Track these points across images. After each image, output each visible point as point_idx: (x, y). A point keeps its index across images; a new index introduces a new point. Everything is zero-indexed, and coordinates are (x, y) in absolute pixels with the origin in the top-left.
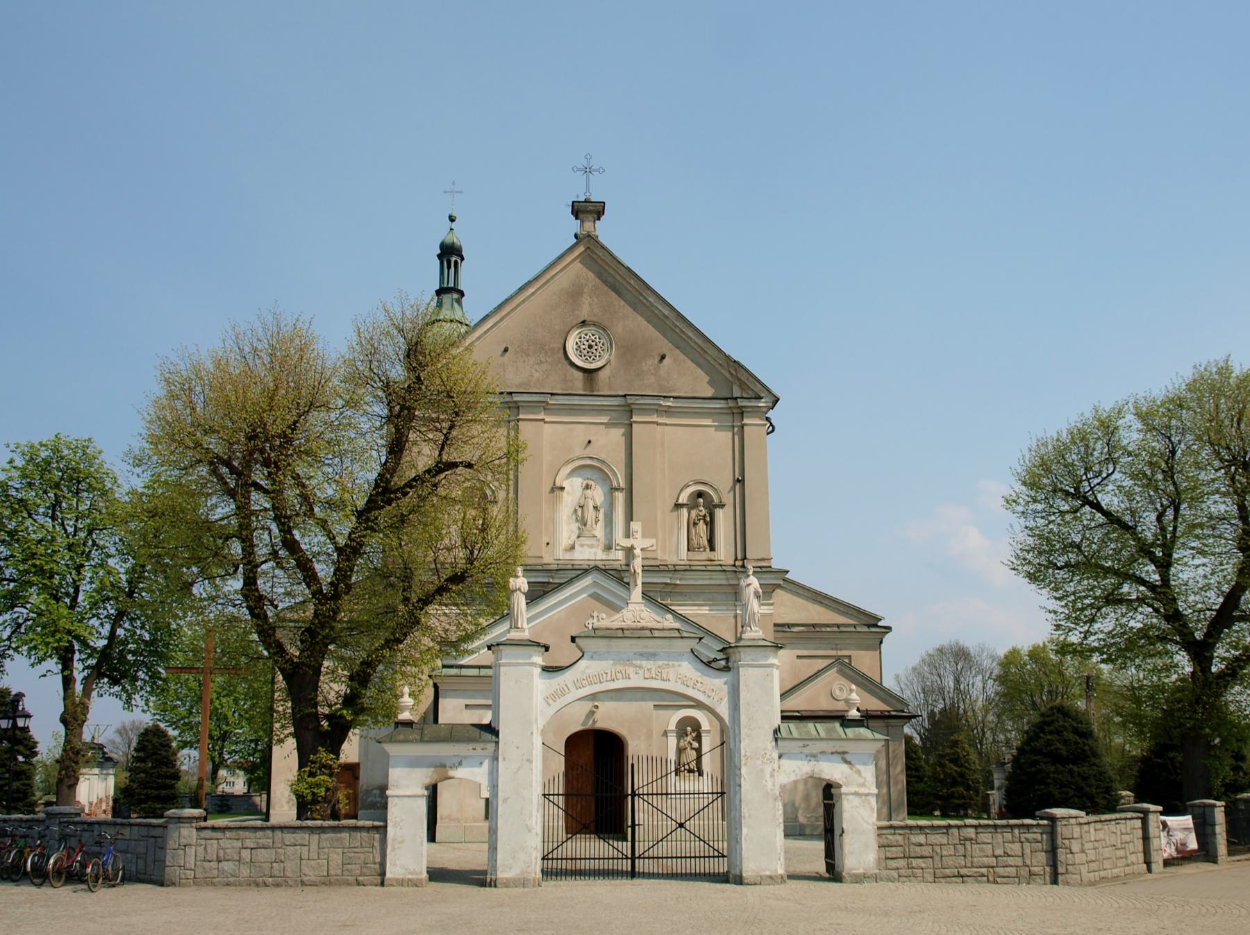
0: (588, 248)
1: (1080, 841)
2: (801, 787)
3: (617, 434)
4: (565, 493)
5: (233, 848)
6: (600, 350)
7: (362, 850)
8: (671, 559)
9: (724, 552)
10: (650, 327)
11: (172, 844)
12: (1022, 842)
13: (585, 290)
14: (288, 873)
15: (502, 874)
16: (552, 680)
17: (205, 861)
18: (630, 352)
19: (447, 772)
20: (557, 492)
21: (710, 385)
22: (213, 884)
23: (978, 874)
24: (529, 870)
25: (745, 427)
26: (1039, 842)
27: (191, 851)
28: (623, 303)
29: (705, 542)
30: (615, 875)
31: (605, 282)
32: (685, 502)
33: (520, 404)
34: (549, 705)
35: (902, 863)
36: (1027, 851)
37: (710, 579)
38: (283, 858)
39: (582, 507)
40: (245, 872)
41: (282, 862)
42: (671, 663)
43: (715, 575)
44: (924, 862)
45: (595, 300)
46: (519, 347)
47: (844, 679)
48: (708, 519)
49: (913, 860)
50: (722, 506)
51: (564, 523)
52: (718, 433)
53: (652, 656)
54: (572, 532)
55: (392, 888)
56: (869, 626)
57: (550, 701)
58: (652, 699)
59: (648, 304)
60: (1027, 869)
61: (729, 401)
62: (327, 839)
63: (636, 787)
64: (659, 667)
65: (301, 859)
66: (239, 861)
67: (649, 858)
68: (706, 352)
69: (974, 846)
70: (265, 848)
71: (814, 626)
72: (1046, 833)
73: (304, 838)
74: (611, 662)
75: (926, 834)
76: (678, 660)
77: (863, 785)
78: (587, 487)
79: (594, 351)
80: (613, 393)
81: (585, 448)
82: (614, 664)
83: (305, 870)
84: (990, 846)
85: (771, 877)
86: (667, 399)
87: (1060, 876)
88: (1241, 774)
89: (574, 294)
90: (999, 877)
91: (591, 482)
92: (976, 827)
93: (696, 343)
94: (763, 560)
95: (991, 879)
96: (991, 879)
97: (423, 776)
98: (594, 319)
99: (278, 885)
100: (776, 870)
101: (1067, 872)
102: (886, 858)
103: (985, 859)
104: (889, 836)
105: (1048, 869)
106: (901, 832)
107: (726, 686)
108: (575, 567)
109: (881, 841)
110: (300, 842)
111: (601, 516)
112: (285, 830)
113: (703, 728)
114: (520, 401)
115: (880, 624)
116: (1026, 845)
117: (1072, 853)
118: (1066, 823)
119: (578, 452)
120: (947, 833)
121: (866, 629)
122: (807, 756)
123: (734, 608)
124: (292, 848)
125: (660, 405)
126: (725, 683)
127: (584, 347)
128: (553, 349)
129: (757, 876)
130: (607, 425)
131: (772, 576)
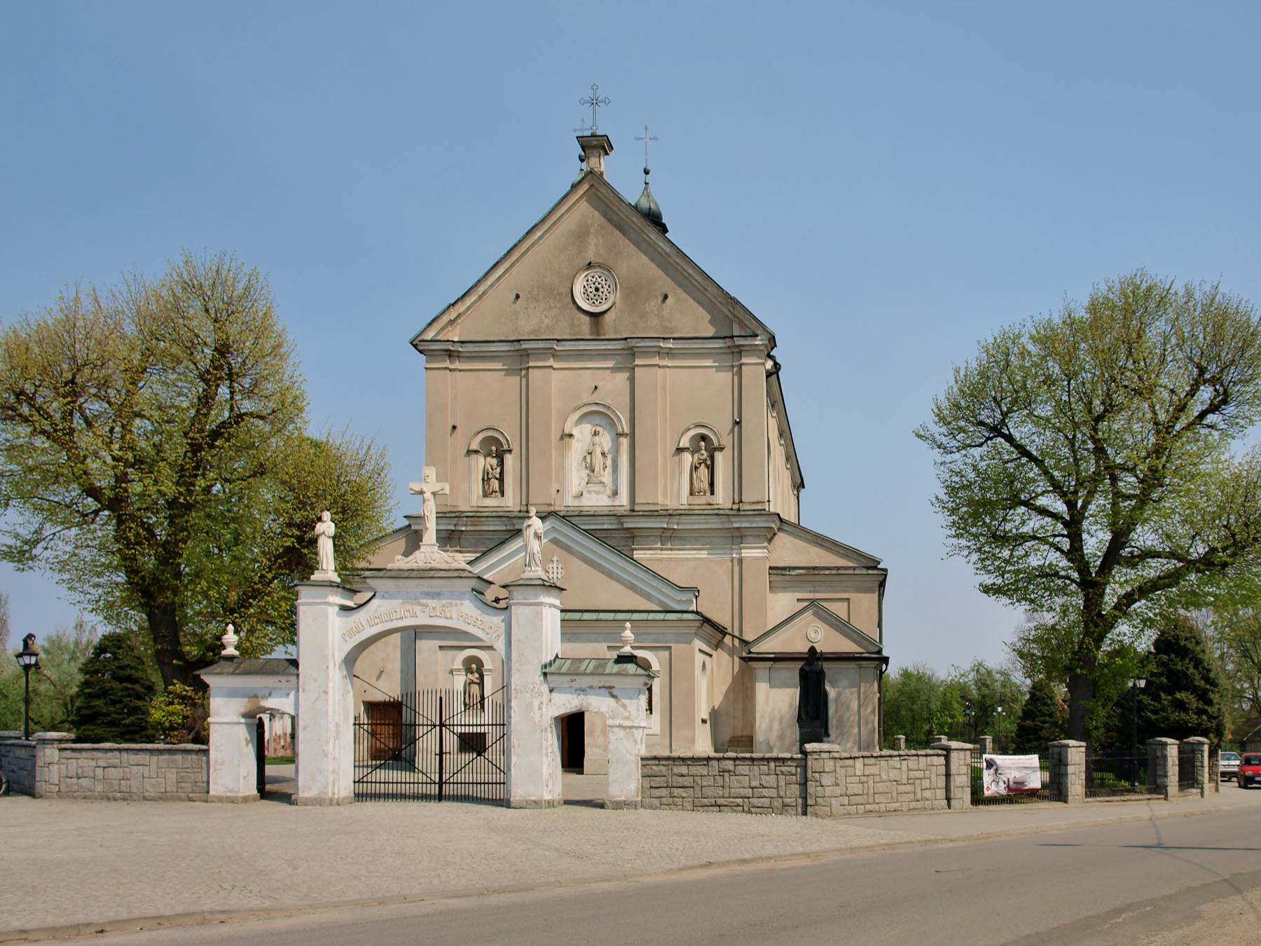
0: (592, 185)
1: (834, 774)
2: (776, 726)
3: (622, 377)
4: (574, 441)
5: (89, 766)
6: (606, 292)
7: (192, 770)
8: (672, 504)
9: (722, 498)
10: (653, 265)
11: (40, 762)
12: (777, 775)
13: (591, 231)
14: (134, 790)
15: (303, 794)
16: (350, 618)
17: (67, 777)
18: (634, 292)
19: (259, 702)
20: (567, 439)
21: (711, 324)
22: (74, 797)
23: (735, 804)
24: (326, 790)
25: (743, 367)
26: (792, 775)
27: (55, 769)
28: (627, 241)
29: (706, 485)
30: (373, 798)
31: (610, 221)
32: (687, 445)
33: (529, 352)
34: (346, 641)
35: (664, 792)
36: (782, 783)
37: (706, 523)
38: (128, 776)
39: (591, 453)
40: (99, 788)
41: (128, 779)
42: (454, 602)
43: (711, 519)
44: (685, 792)
45: (601, 241)
46: (529, 293)
47: (820, 621)
48: (709, 462)
49: (675, 789)
50: (721, 449)
51: (574, 469)
52: (721, 374)
53: (437, 595)
54: (582, 479)
55: (213, 804)
56: (868, 568)
57: (347, 638)
58: (605, 641)
59: (651, 242)
60: (780, 800)
61: (727, 340)
62: (164, 760)
63: (444, 719)
64: (443, 606)
65: (143, 777)
66: (94, 778)
67: (367, 782)
68: (706, 289)
69: (732, 778)
70: (115, 767)
71: (814, 568)
72: (800, 766)
73: (145, 759)
74: (400, 601)
75: (688, 765)
76: (460, 599)
77: (628, 718)
78: (596, 434)
79: (600, 294)
80: (618, 337)
81: (593, 393)
82: (403, 604)
83: (147, 787)
84: (747, 778)
85: (535, 802)
86: (666, 341)
87: (808, 808)
88: (1204, 717)
89: (581, 235)
90: (754, 807)
91: (598, 429)
92: (734, 759)
93: (696, 281)
94: (758, 503)
95: (746, 809)
96: (746, 809)
97: (241, 705)
98: (600, 260)
99: (124, 799)
100: (542, 796)
101: (816, 804)
102: (651, 787)
103: (742, 790)
104: (653, 767)
105: (800, 801)
106: (664, 763)
107: (503, 624)
108: (582, 513)
109: (646, 771)
110: (142, 762)
111: (609, 463)
112: (130, 752)
113: (486, 667)
114: (530, 349)
115: (879, 567)
116: (781, 777)
117: (821, 786)
118: (817, 757)
119: (586, 398)
120: (708, 765)
121: (864, 571)
122: (576, 690)
123: (730, 552)
124: (135, 767)
125: (661, 347)
126: (503, 621)
127: (590, 290)
128: (560, 294)
129: (523, 801)
130: (613, 369)
131: (763, 519)
